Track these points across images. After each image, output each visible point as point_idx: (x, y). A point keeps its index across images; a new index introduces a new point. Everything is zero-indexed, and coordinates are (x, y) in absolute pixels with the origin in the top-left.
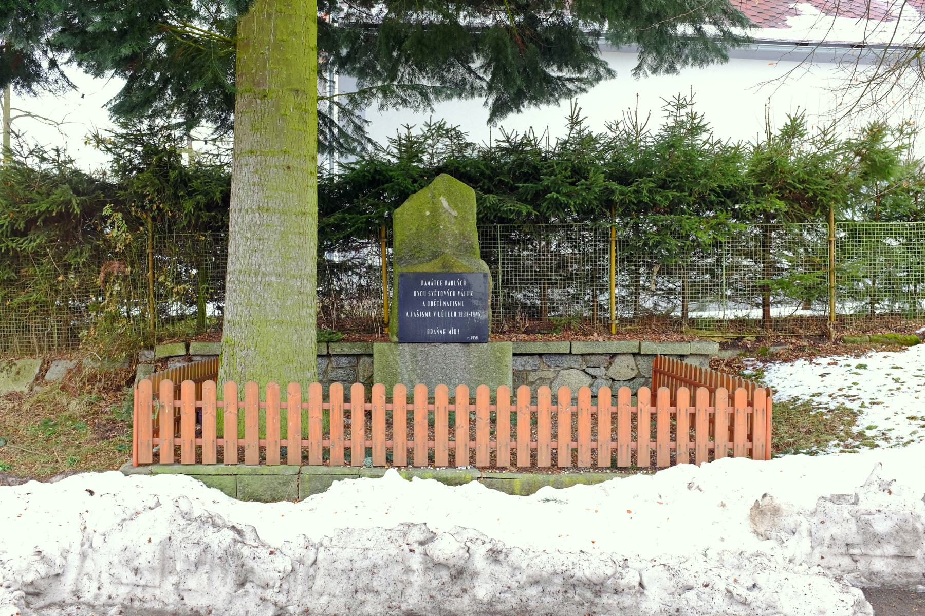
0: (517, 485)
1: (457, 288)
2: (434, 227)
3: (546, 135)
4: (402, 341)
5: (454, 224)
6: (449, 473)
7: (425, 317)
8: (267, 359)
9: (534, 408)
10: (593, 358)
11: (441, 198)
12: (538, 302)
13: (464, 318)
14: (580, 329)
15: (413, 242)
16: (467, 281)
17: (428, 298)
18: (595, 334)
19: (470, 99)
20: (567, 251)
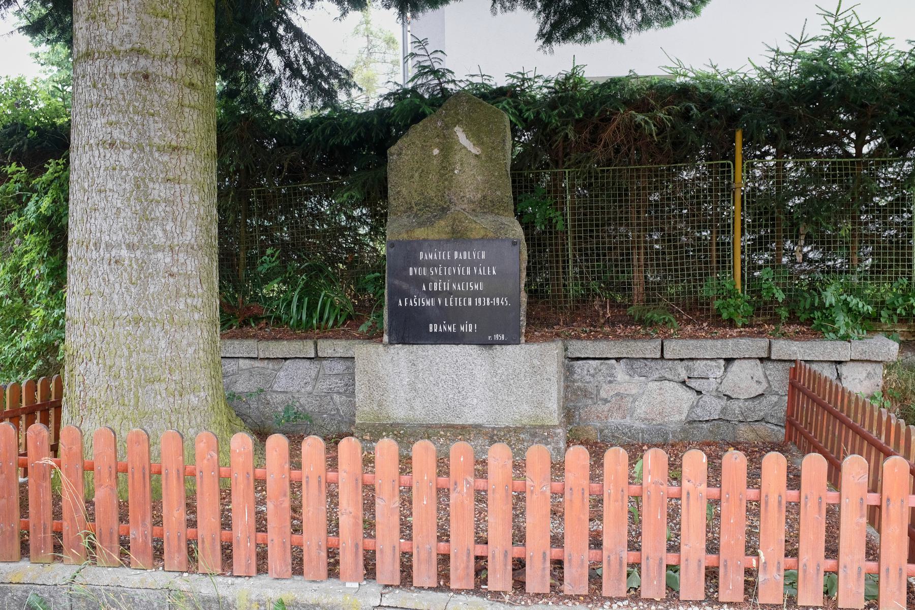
1: (472, 263)
8: (117, 377)
13: (483, 308)
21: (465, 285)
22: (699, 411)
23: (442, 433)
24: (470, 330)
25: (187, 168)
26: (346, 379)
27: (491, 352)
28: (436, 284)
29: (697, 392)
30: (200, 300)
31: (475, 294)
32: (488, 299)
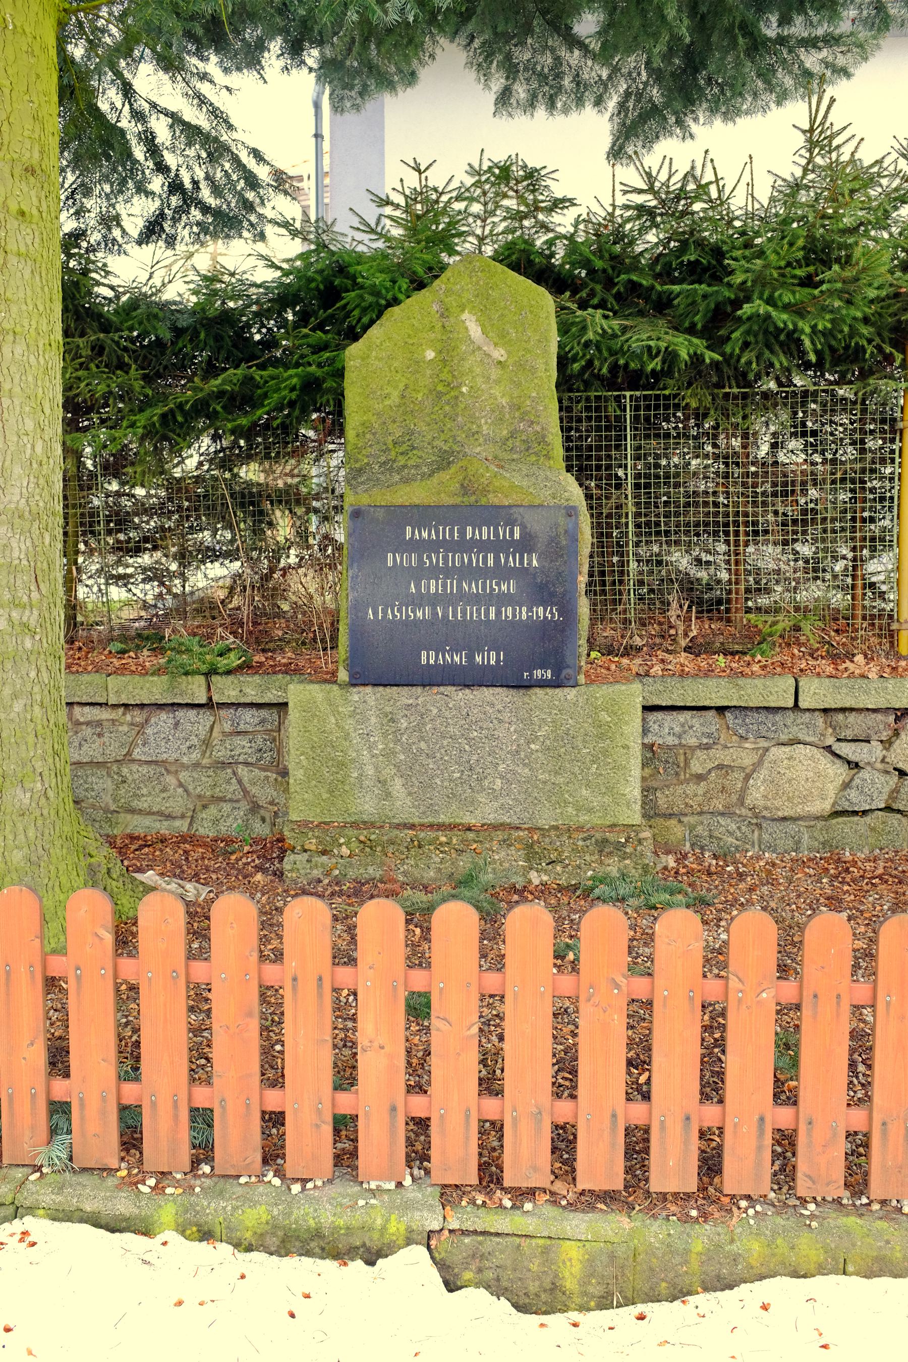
0: (572, 1263)
1: (497, 546)
2: (445, 391)
3: (746, 178)
4: (357, 681)
5: (498, 382)
6: (327, 1207)
7: (416, 622)
9: (640, 987)
10: (852, 718)
11: (465, 316)
12: (724, 576)
14: (823, 642)
15: (392, 427)
16: (523, 528)
17: (419, 573)
18: (859, 658)
19: (574, 116)
20: (794, 456)
21: (484, 584)
22: (853, 794)
23: (443, 839)
24: (492, 662)
25: (13, 369)
26: (260, 741)
27: (526, 699)
28: (433, 582)
29: (849, 763)
30: (36, 612)
31: (503, 600)
32: (524, 609)
